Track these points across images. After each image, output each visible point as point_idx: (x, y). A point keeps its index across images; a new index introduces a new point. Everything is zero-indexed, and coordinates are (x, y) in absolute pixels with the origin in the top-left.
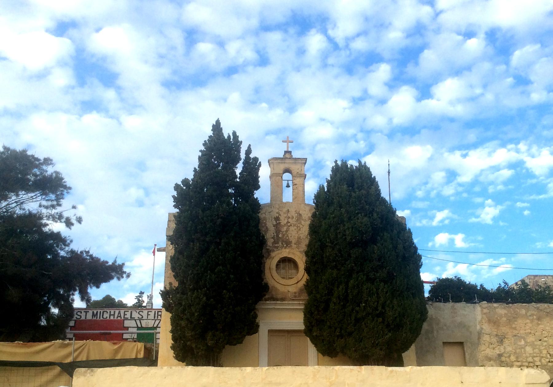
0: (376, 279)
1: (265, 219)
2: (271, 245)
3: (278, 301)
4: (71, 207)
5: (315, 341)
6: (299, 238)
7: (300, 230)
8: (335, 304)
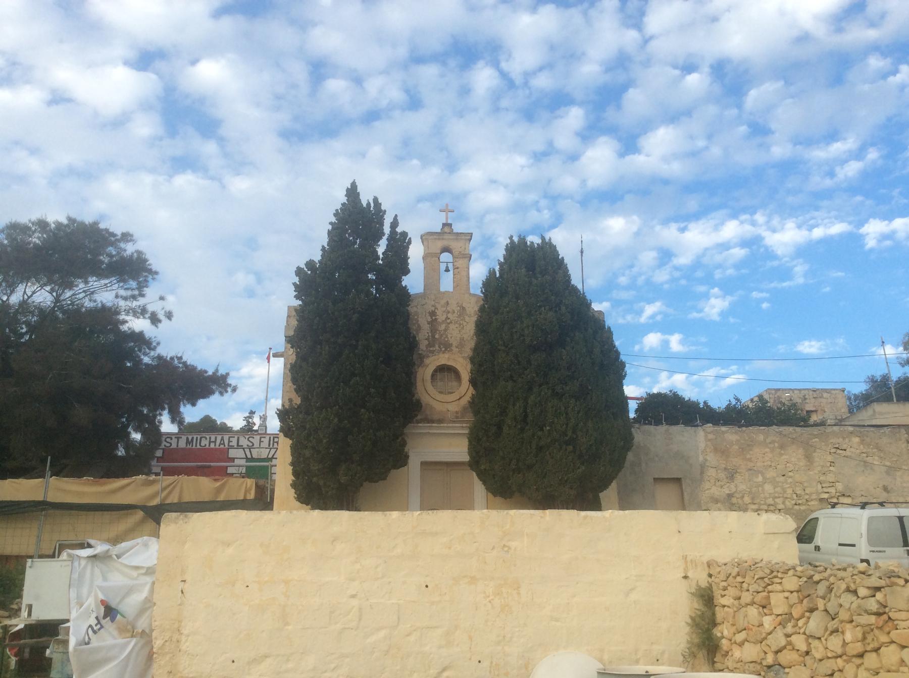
5: (482, 476)
6: (462, 339)
7: (463, 328)
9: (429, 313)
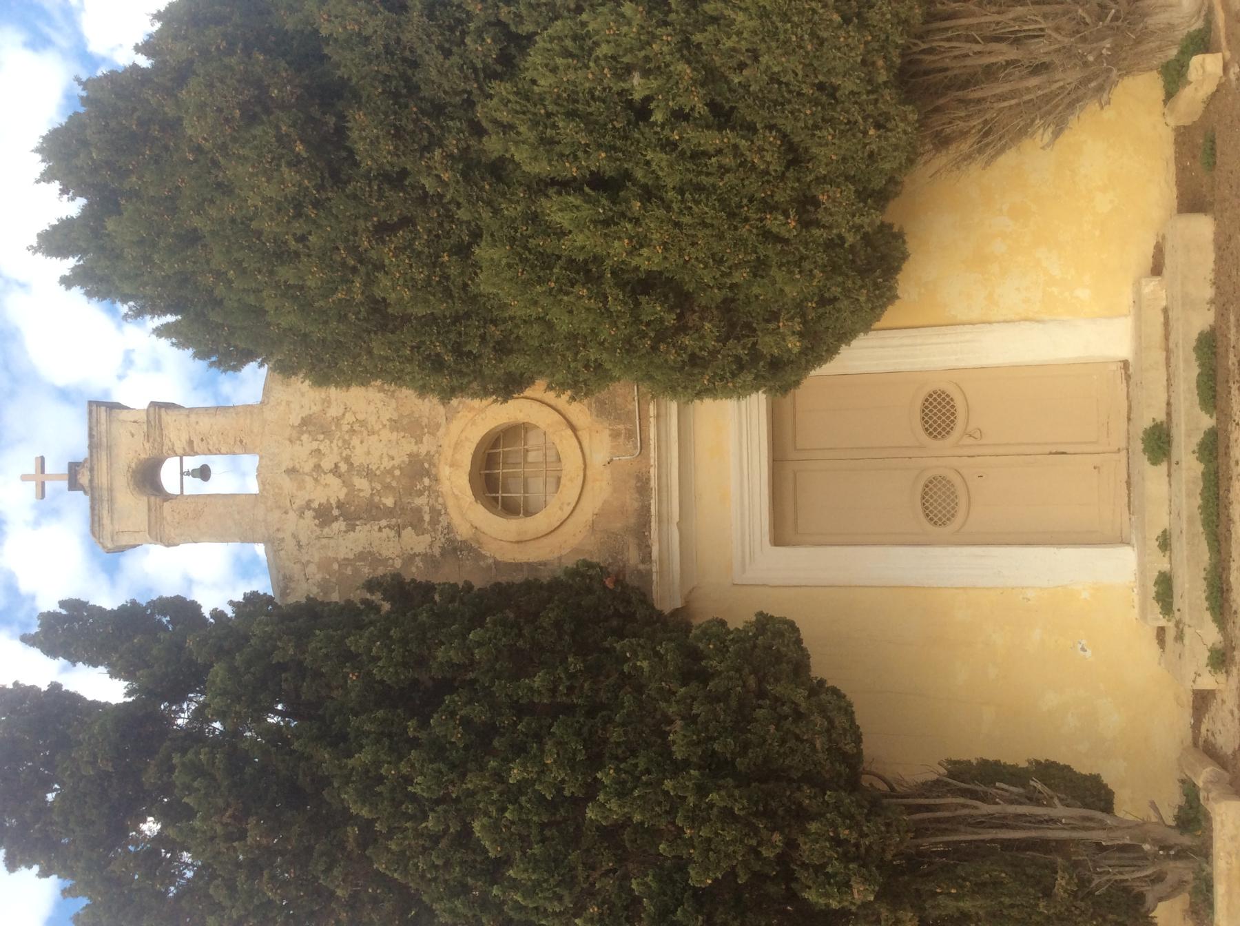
0: (499, 23)
1: (324, 565)
2: (427, 538)
3: (649, 510)
5: (821, 342)
6: (395, 425)
7: (363, 423)
8: (640, 243)
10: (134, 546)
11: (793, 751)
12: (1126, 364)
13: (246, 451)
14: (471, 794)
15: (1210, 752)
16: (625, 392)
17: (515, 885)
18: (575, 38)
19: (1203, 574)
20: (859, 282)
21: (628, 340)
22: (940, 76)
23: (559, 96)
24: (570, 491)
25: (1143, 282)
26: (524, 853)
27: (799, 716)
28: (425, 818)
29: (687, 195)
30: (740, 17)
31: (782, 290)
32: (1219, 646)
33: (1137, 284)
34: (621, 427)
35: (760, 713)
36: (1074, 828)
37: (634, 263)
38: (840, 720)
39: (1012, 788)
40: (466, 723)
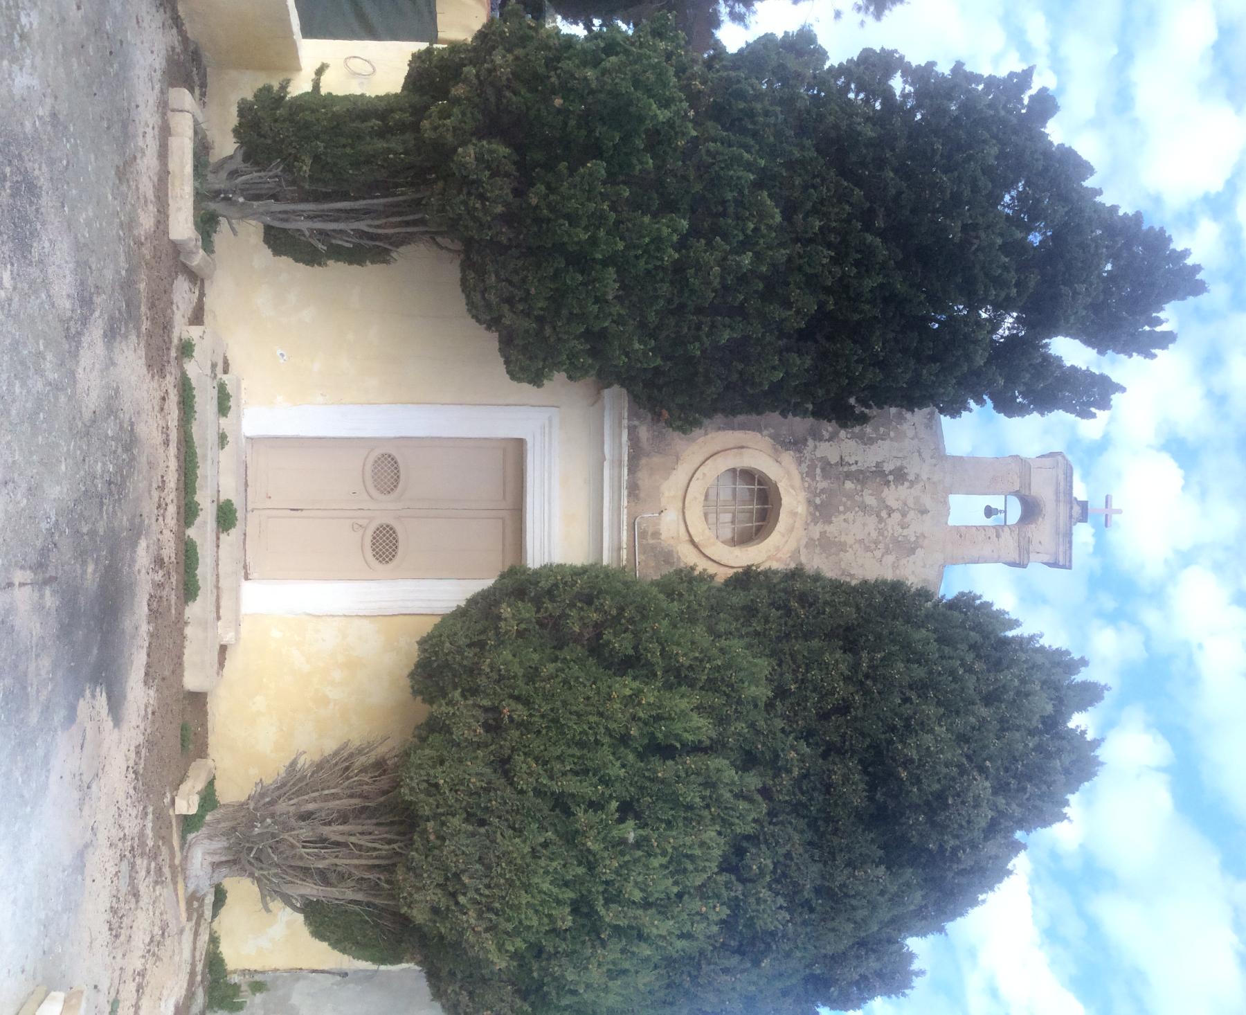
0: (743, 881)
4: (839, 7)
5: (481, 610)
7: (867, 549)
9: (901, 469)
10: (1043, 456)
11: (516, 272)
12: (247, 578)
13: (957, 528)
14: (782, 245)
15: (195, 278)
16: (648, 571)
17: (749, 167)
18: (685, 871)
19: (197, 416)
20: (449, 658)
21: (644, 617)
22: (382, 820)
23: (699, 823)
24: (697, 490)
25: (233, 641)
26: (741, 192)
27: (509, 301)
28: (821, 228)
29: (592, 739)
30: (545, 886)
31: (514, 656)
32: (186, 360)
33: (237, 639)
34: (651, 542)
35: (541, 304)
36: (294, 212)
37: (637, 683)
38: (477, 297)
39: (340, 242)
40: (787, 304)
